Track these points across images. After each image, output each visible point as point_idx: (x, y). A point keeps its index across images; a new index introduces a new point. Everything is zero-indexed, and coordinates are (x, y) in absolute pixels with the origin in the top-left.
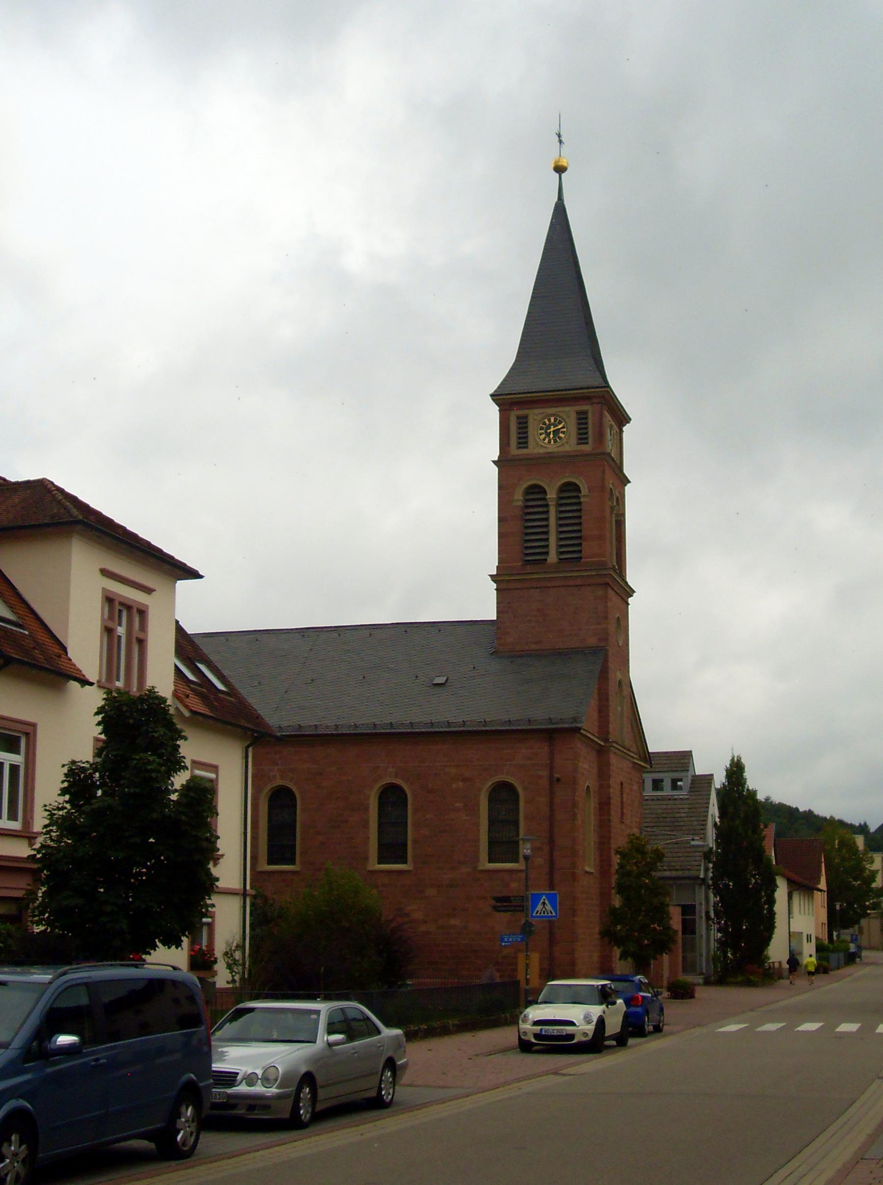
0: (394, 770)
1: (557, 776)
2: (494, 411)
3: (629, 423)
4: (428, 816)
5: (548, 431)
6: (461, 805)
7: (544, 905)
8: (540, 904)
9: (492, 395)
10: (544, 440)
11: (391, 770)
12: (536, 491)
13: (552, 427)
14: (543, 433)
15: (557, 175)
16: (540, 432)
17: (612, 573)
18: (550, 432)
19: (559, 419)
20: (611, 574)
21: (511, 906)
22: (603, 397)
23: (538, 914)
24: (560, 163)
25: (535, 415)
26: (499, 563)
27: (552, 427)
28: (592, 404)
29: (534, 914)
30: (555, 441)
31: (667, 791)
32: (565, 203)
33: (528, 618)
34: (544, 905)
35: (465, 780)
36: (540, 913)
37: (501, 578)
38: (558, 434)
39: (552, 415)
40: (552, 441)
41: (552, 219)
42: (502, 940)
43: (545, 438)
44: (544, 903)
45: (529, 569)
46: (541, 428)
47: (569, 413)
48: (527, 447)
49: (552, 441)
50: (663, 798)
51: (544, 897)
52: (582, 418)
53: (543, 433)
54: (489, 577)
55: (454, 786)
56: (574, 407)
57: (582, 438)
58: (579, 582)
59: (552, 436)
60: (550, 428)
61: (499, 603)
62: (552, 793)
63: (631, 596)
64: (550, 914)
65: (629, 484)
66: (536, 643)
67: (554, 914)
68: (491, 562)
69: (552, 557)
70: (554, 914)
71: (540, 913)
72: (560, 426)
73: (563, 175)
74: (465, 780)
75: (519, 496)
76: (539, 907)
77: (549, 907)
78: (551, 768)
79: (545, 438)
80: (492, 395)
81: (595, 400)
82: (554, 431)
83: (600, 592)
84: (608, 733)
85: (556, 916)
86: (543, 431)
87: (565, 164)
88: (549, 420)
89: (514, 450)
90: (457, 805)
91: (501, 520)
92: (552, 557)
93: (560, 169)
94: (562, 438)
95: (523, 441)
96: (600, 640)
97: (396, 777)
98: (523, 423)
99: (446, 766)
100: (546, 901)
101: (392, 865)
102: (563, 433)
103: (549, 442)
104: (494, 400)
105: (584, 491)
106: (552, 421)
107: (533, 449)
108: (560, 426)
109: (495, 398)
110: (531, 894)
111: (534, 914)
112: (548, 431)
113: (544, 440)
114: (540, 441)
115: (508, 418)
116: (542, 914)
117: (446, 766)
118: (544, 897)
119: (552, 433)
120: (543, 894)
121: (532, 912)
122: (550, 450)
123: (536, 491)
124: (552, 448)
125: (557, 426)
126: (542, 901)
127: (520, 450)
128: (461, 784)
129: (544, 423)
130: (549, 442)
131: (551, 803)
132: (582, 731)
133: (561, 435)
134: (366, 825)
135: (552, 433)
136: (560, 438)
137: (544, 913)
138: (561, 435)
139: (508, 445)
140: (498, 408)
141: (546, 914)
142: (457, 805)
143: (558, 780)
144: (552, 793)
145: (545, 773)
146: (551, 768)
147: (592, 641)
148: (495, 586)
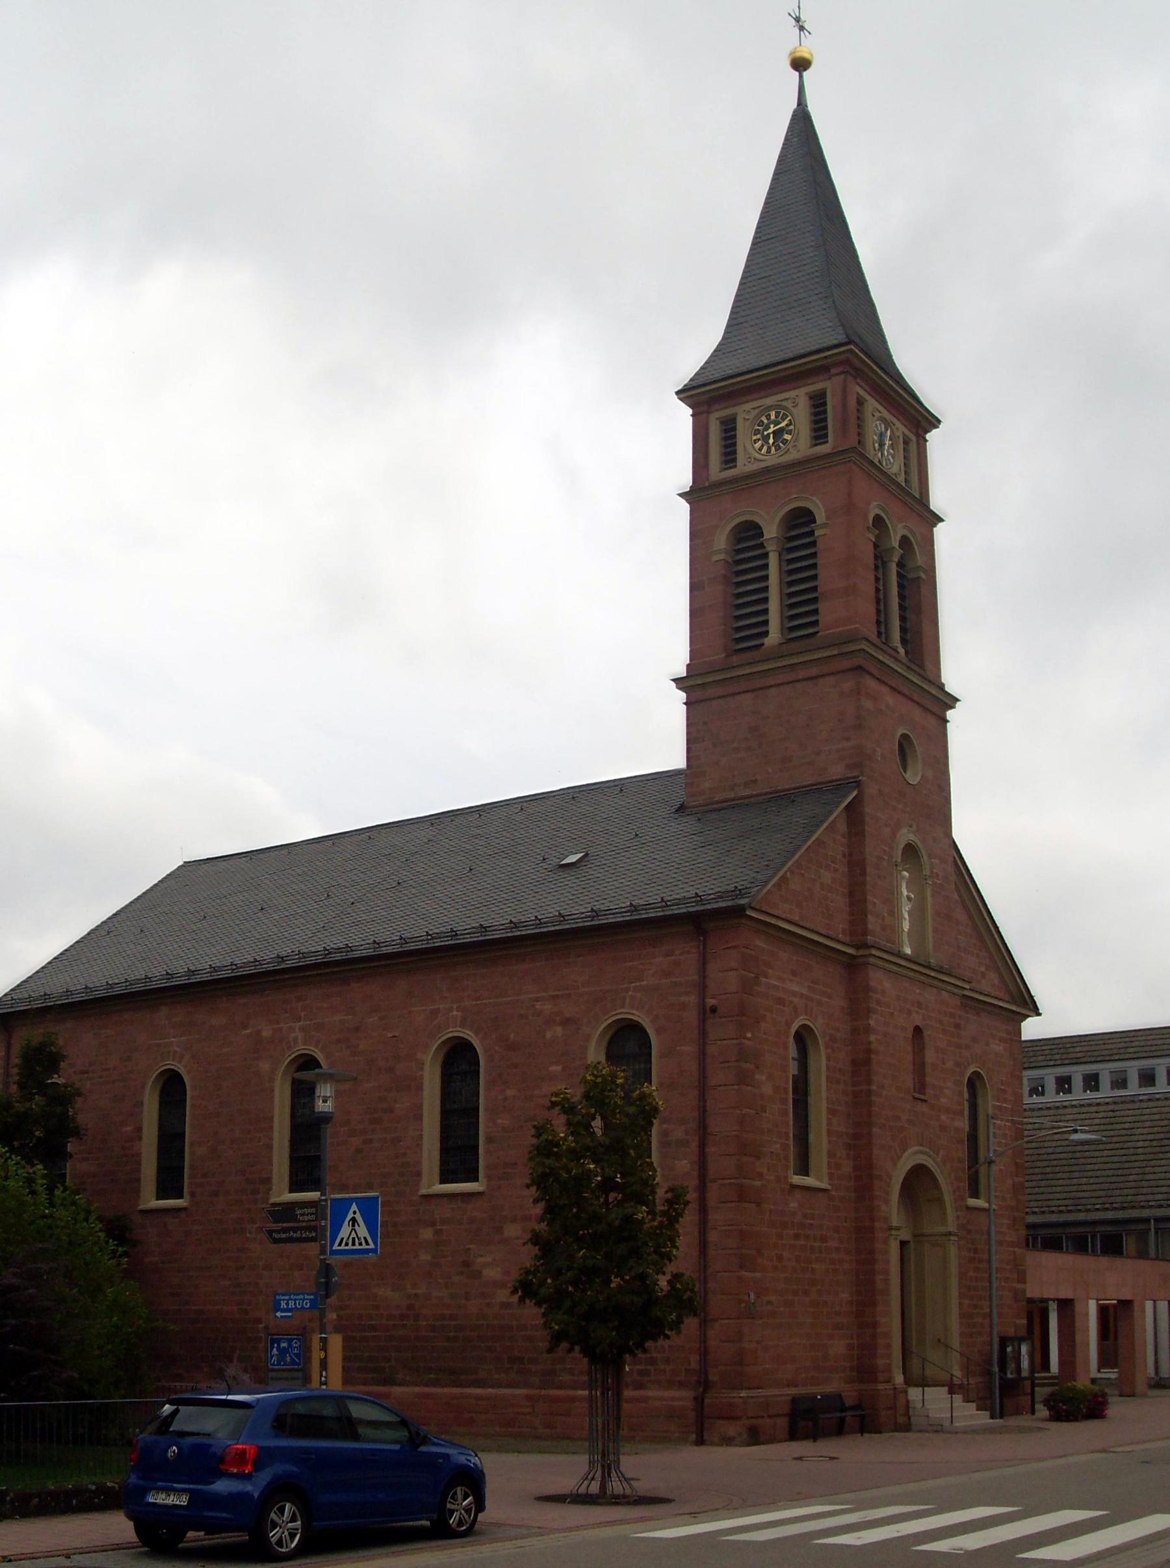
0: (459, 1013)
1: (711, 1002)
2: (684, 414)
3: (937, 427)
4: (509, 1093)
5: (766, 433)
6: (559, 1068)
7: (353, 1225)
8: (346, 1222)
9: (678, 393)
10: (760, 449)
11: (455, 1013)
12: (748, 532)
13: (772, 426)
14: (759, 440)
15: (797, 73)
16: (755, 438)
17: (864, 646)
18: (769, 434)
19: (782, 412)
20: (864, 650)
21: (295, 1230)
22: (847, 362)
23: (343, 1247)
24: (798, 54)
25: (745, 412)
26: (691, 660)
27: (772, 426)
28: (830, 379)
29: (335, 1247)
30: (778, 448)
31: (1133, 1088)
32: (810, 109)
33: (735, 745)
34: (353, 1225)
35: (567, 1022)
36: (347, 1244)
37: (692, 683)
38: (783, 435)
39: (769, 408)
40: (773, 448)
41: (787, 133)
42: (277, 1308)
43: (763, 446)
44: (354, 1220)
45: (735, 659)
46: (757, 432)
47: (798, 401)
48: (735, 466)
49: (773, 448)
50: (1133, 1099)
51: (354, 1207)
52: (818, 403)
53: (759, 440)
54: (673, 683)
55: (548, 1035)
56: (802, 389)
57: (819, 433)
58: (814, 671)
59: (771, 441)
60: (770, 428)
61: (689, 725)
62: (703, 1033)
63: (952, 707)
64: (364, 1246)
65: (940, 525)
66: (746, 785)
67: (372, 1246)
68: (678, 659)
69: (774, 635)
70: (372, 1246)
71: (347, 1244)
72: (783, 425)
73: (805, 74)
74: (567, 1022)
75: (721, 541)
76: (345, 1231)
77: (362, 1231)
78: (702, 987)
79: (763, 446)
80: (678, 393)
81: (833, 371)
82: (774, 432)
83: (848, 684)
84: (865, 932)
85: (374, 1251)
86: (759, 436)
87: (807, 55)
88: (768, 417)
89: (716, 472)
90: (553, 1068)
91: (694, 587)
92: (774, 635)
93: (800, 64)
94: (787, 440)
95: (729, 456)
96: (849, 767)
97: (463, 1025)
98: (729, 429)
99: (537, 1000)
100: (358, 1217)
101: (186, 1153)
102: (789, 432)
103: (769, 449)
104: (681, 399)
105: (820, 516)
106: (773, 417)
107: (743, 466)
108: (783, 425)
109: (682, 396)
110: (331, 1200)
111: (335, 1247)
112: (766, 433)
113: (760, 449)
114: (754, 452)
115: (706, 428)
116: (350, 1247)
117: (537, 1000)
118: (354, 1207)
119: (771, 436)
120: (352, 1200)
121: (332, 1246)
122: (769, 464)
123: (748, 532)
124: (774, 459)
125: (780, 423)
126: (350, 1215)
127: (726, 471)
128: (559, 1030)
129: (761, 423)
130: (769, 451)
131: (702, 1055)
132: (748, 913)
133: (787, 437)
134: (417, 1115)
135: (771, 436)
136: (785, 442)
137: (354, 1244)
138: (787, 437)
139: (706, 466)
140: (690, 411)
141: (357, 1247)
142: (553, 1068)
143: (714, 1010)
144: (703, 1033)
145: (693, 999)
146: (702, 987)
147: (837, 771)
148: (682, 696)
